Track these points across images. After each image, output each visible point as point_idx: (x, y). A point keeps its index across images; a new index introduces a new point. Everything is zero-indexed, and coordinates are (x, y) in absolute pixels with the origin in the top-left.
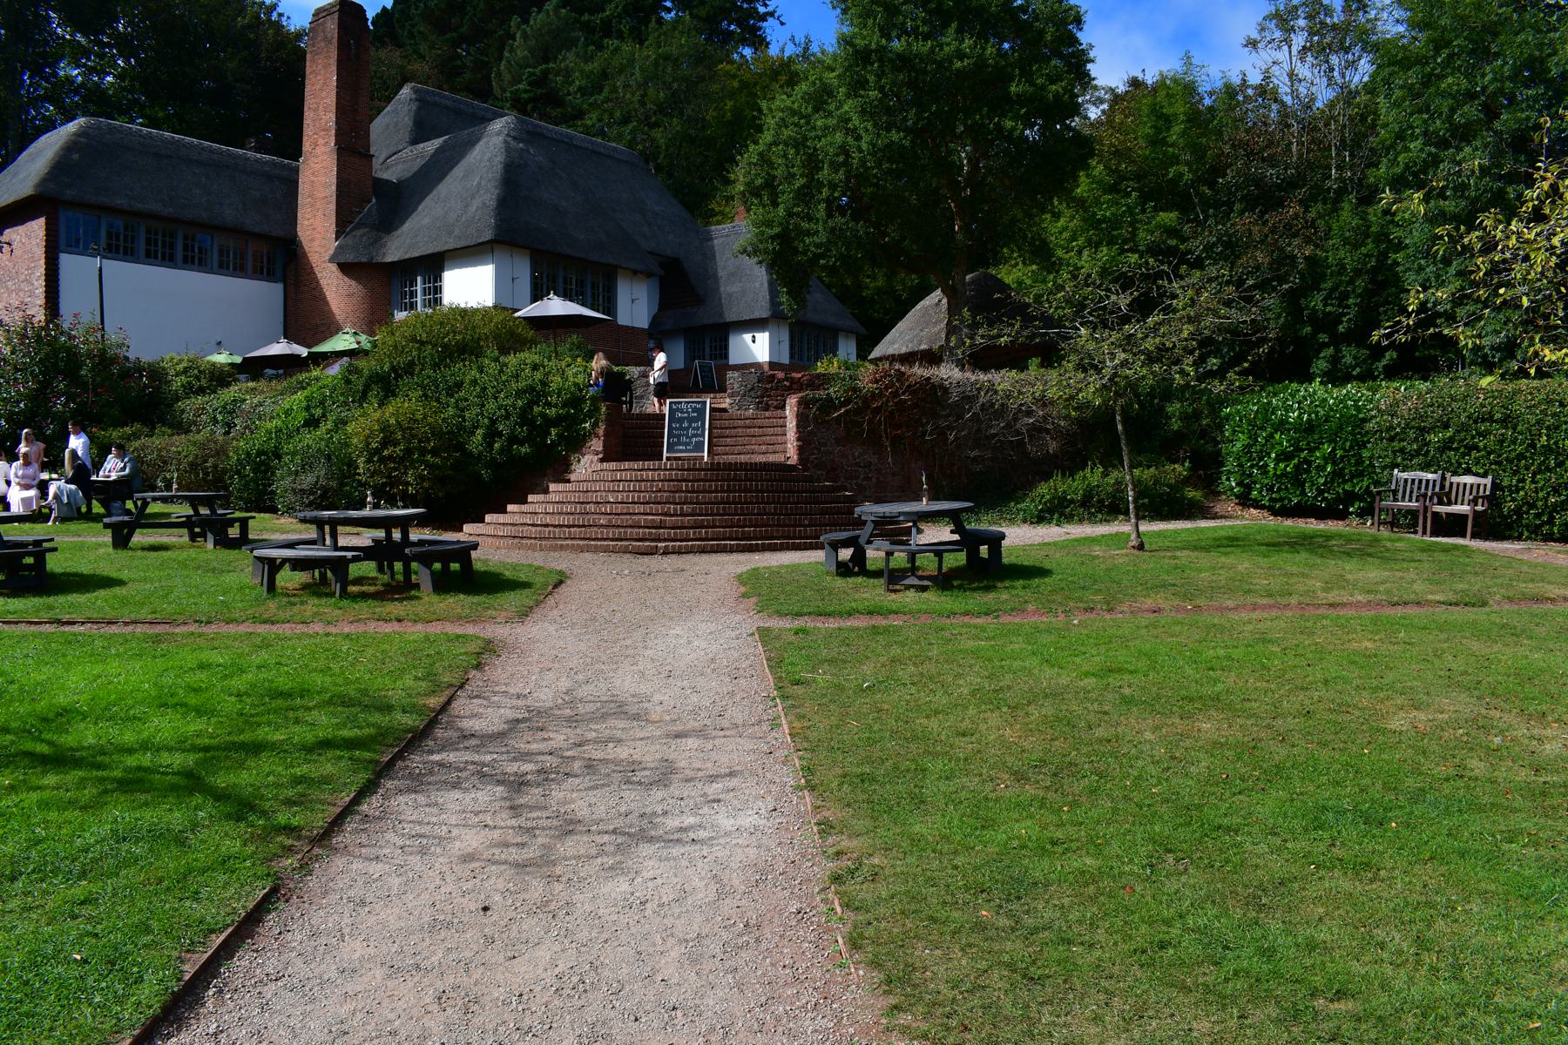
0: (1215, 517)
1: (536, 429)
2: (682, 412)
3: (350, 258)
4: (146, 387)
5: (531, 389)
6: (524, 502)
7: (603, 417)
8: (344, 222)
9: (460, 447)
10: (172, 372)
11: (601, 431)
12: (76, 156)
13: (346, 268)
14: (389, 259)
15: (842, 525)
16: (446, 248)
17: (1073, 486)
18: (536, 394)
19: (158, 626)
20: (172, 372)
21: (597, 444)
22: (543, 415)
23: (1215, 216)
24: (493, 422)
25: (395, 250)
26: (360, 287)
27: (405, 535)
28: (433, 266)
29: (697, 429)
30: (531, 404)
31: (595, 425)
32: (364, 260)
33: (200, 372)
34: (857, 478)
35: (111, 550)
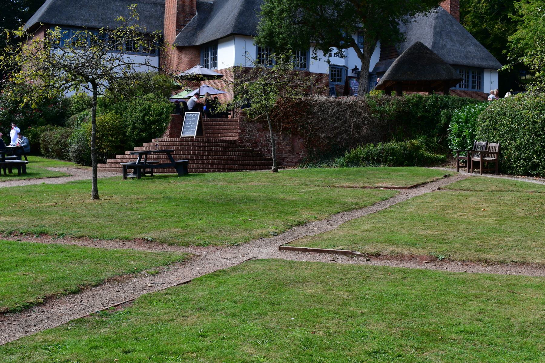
0: (32, 175)
1: (147, 124)
2: (190, 118)
3: (181, 44)
4: (60, 109)
5: (145, 109)
7: (170, 121)
8: (180, 26)
9: (124, 134)
10: (73, 102)
11: (169, 126)
13: (179, 48)
14: (198, 44)
15: (230, 169)
16: (217, 38)
17: (362, 151)
18: (146, 111)
20: (73, 102)
22: (149, 120)
25: (203, 38)
26: (186, 58)
27: (144, 170)
29: (194, 125)
30: (145, 115)
31: (167, 124)
32: (186, 45)
33: (84, 102)
34: (268, 146)
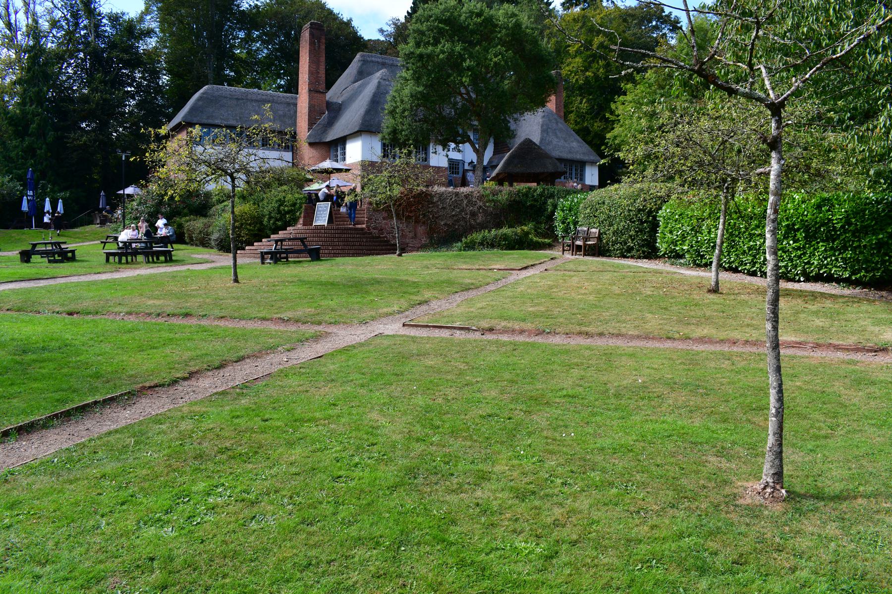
3: (312, 141)
6: (261, 241)
11: (302, 215)
12: (200, 103)
14: (328, 140)
17: (477, 236)
18: (281, 202)
19: (42, 281)
21: (301, 221)
23: (417, 67)
24: (270, 213)
25: (333, 134)
28: (342, 142)
30: (280, 206)
32: (317, 141)
35: (18, 263)
